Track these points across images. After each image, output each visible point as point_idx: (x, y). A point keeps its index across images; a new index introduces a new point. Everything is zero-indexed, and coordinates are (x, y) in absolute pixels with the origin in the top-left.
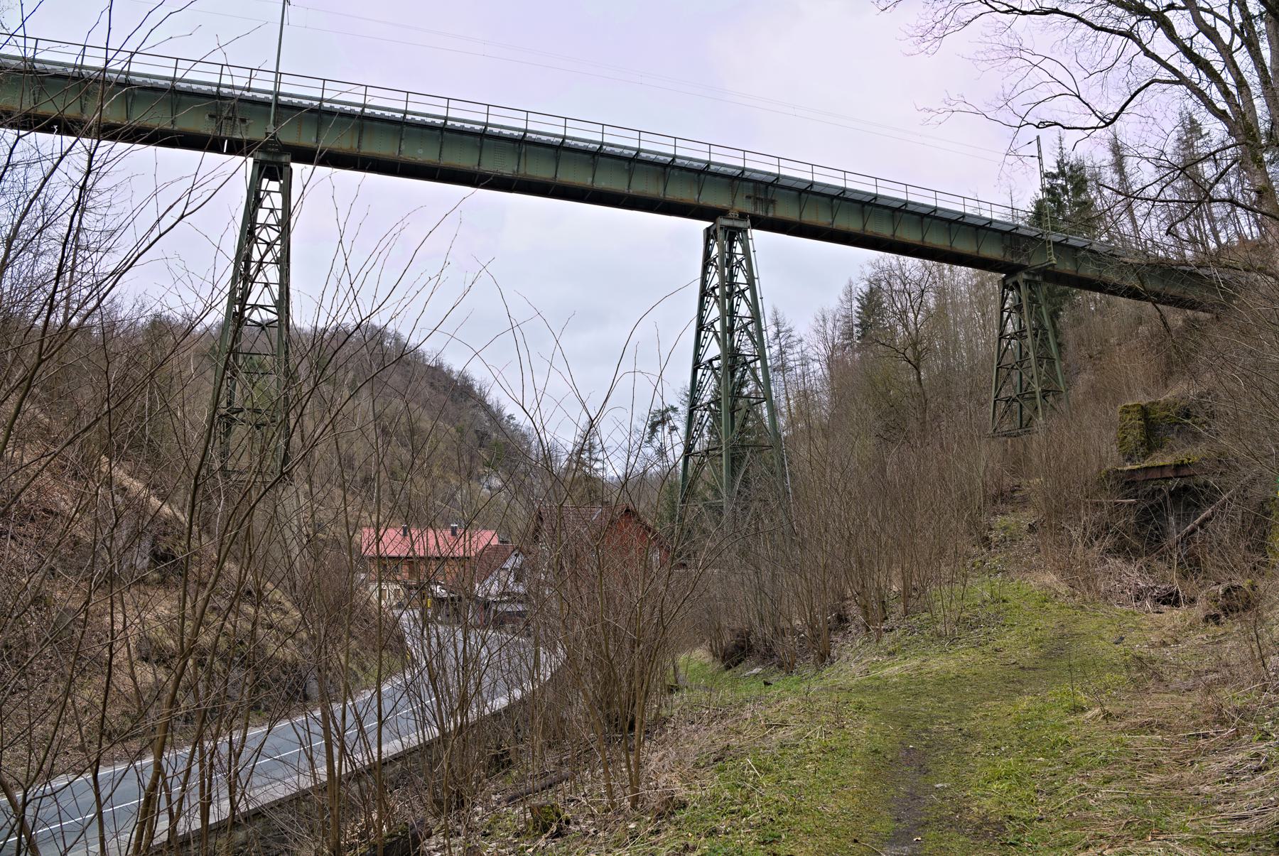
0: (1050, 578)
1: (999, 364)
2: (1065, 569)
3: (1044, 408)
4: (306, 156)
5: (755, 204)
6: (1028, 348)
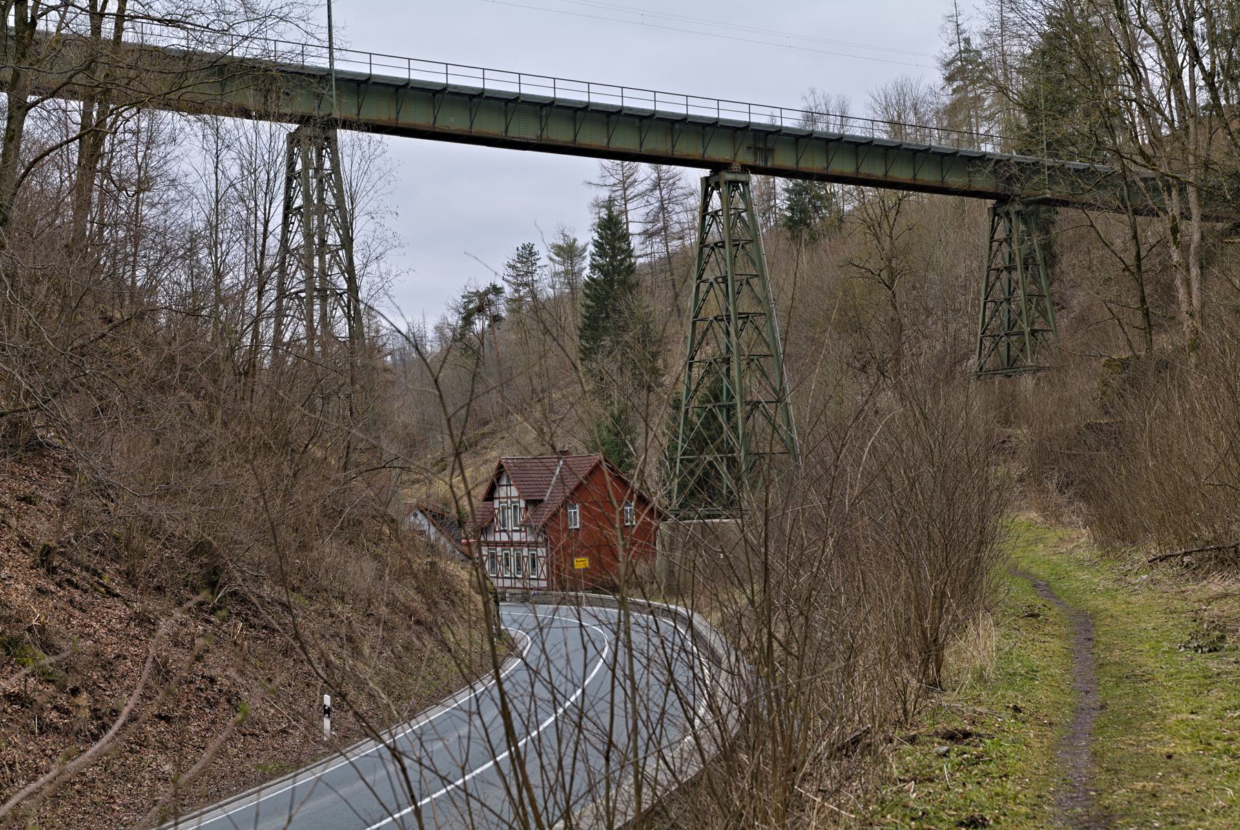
0: (1033, 515)
1: (986, 299)
2: (1043, 510)
3: (1033, 346)
4: (347, 125)
5: (755, 154)
6: (1017, 283)
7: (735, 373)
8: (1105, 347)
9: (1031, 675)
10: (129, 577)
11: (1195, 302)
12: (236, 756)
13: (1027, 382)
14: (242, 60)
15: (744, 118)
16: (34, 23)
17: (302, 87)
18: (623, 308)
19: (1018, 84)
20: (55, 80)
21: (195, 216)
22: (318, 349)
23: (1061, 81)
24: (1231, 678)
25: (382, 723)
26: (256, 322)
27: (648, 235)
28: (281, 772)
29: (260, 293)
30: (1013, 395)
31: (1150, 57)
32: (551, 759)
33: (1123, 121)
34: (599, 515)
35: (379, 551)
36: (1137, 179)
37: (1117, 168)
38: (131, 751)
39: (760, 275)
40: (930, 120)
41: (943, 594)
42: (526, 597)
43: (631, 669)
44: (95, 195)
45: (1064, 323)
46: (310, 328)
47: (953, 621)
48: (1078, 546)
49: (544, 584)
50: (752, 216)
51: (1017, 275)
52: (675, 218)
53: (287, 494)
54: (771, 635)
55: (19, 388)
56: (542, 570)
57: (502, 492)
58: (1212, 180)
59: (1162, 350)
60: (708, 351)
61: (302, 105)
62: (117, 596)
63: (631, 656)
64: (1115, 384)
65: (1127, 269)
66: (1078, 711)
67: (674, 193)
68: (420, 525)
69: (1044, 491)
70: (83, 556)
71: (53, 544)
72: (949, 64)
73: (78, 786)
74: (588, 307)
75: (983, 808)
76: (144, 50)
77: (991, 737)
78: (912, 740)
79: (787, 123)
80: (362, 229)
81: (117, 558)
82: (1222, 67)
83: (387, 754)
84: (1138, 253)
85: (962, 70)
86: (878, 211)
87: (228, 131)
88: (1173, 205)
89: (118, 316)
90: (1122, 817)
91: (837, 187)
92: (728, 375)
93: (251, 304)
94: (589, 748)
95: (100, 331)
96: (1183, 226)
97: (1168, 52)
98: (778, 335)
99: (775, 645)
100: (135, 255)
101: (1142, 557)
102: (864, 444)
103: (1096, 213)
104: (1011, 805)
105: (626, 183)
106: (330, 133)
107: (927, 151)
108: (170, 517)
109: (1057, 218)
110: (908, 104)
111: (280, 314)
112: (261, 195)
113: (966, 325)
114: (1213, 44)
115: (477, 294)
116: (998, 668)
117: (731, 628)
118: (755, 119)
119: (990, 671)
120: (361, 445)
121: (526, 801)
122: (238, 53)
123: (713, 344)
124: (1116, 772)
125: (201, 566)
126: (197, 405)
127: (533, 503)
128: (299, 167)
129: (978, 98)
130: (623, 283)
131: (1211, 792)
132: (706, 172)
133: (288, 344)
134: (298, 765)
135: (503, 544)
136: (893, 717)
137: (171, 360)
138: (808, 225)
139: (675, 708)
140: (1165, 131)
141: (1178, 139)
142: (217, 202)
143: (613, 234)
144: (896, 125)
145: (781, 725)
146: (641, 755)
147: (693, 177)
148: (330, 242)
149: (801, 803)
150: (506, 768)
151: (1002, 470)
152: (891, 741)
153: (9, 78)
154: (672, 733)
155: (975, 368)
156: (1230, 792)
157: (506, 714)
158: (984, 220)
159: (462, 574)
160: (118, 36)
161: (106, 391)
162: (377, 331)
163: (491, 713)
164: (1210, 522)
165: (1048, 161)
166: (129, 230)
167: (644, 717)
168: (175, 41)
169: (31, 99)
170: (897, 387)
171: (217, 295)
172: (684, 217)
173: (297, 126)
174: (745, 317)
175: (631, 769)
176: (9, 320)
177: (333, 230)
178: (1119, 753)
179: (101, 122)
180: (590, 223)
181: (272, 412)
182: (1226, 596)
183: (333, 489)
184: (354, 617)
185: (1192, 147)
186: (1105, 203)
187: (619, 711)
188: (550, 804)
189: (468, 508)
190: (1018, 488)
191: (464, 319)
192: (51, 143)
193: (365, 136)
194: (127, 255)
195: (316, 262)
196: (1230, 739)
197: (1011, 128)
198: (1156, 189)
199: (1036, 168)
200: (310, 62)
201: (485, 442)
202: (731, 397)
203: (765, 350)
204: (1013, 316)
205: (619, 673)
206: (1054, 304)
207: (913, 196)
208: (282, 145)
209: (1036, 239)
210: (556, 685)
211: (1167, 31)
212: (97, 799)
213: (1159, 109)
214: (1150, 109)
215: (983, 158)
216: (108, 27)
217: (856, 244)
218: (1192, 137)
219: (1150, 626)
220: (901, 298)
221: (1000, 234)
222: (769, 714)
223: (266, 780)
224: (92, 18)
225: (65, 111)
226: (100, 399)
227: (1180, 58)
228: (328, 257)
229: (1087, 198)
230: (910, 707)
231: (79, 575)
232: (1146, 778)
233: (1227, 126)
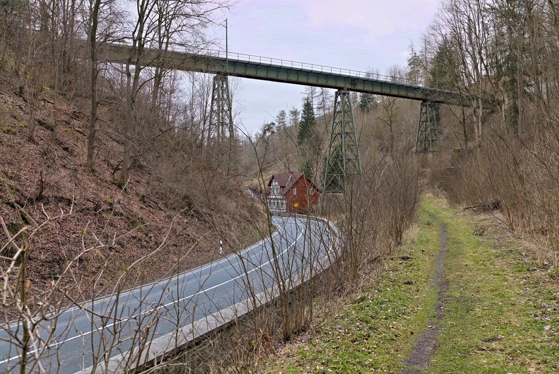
2: (433, 193)
3: (432, 145)
4: (231, 74)
7: (343, 150)
8: (453, 146)
9: (428, 241)
10: (166, 205)
11: (480, 133)
12: (195, 257)
13: (430, 155)
14: (201, 55)
15: (348, 74)
16: (143, 45)
17: (218, 63)
18: (311, 130)
19: (430, 67)
20: (149, 61)
21: (186, 100)
22: (220, 140)
23: (443, 66)
24: (485, 243)
25: (237, 249)
26: (203, 132)
27: (319, 108)
28: (207, 262)
29: (204, 123)
30: (426, 159)
31: (469, 60)
32: (286, 261)
33: (461, 78)
34: (302, 191)
35: (237, 200)
36: (464, 96)
37: (459, 92)
38: (166, 254)
39: (352, 121)
40: (404, 76)
41: (403, 217)
42: (279, 215)
43: (310, 236)
44: (159, 94)
45: (441, 138)
46: (219, 134)
47: (406, 225)
48: (443, 204)
49: (285, 211)
50: (350, 103)
51: (428, 123)
52: (327, 103)
53: (211, 182)
54: (352, 227)
55: (136, 150)
56: (285, 206)
57: (273, 184)
58: (486, 97)
59: (470, 147)
60: (336, 143)
61: (218, 69)
62: (162, 210)
63: (310, 232)
64: (456, 157)
65: (460, 122)
66: (441, 252)
67: (327, 96)
68: (249, 192)
69: (434, 188)
70: (153, 198)
71: (145, 195)
72: (409, 60)
73: (151, 263)
74: (300, 129)
75: (412, 279)
76: (173, 53)
77: (415, 259)
78: (392, 259)
79: (361, 76)
80: (234, 105)
81: (162, 199)
82: (490, 64)
83: (238, 258)
84: (464, 118)
85: (413, 62)
86: (388, 103)
87: (196, 76)
88: (474, 104)
89: (164, 129)
90: (452, 282)
91: (375, 96)
92: (341, 150)
93: (202, 127)
94: (297, 258)
95: (159, 134)
96: (477, 110)
97: (474, 59)
98: (357, 139)
99: (353, 230)
100: (169, 112)
101: (462, 208)
102: (381, 172)
103: (452, 106)
104: (420, 278)
105: (312, 93)
106: (226, 77)
107: (402, 85)
108: (177, 188)
109: (441, 107)
110: (397, 72)
111: (210, 129)
112: (205, 95)
113: (412, 138)
114: (487, 57)
115: (268, 125)
116: (418, 239)
117: (340, 226)
118: (352, 75)
119: (416, 240)
120: (232, 169)
121: (278, 272)
122: (200, 53)
123: (337, 141)
124: (451, 269)
125: (186, 202)
126: (185, 156)
127: (283, 187)
128: (216, 87)
129: (418, 70)
130: (311, 123)
131: (478, 276)
132: (337, 90)
133: (212, 138)
134: (212, 260)
135: (273, 199)
136: (387, 252)
137: (179, 142)
138: (367, 107)
139: (322, 248)
140: (473, 82)
141: (476, 84)
142: (193, 97)
143: (309, 108)
144: (393, 77)
145: (354, 253)
146: (312, 260)
147: (333, 91)
148: (225, 109)
149: (359, 276)
150: (273, 263)
151: (422, 181)
152: (386, 259)
153: (136, 61)
154: (322, 255)
155: (415, 151)
156: (483, 276)
157: (273, 247)
158: (419, 106)
159: (261, 207)
160: (166, 49)
161: (160, 151)
162: (238, 135)
163: (269, 247)
164: (482, 198)
165: (438, 90)
166: (167, 104)
167: (313, 250)
168: (182, 50)
169: (142, 67)
170: (392, 155)
171: (192, 124)
172: (329, 103)
173: (216, 75)
174: (347, 134)
175: (309, 265)
176: (134, 130)
177: (226, 105)
178: (452, 264)
179: (161, 73)
180: (302, 104)
181: (207, 158)
182: (485, 220)
183: (224, 181)
184: (229, 219)
185: (480, 87)
186: (454, 102)
187: (306, 248)
188: (285, 273)
189: (264, 188)
190: (426, 186)
191: (263, 132)
192: (147, 80)
193: (236, 78)
194: (167, 112)
195: (221, 115)
196: (484, 261)
197: (428, 79)
198: (470, 99)
199: (435, 92)
200: (220, 56)
201: (268, 169)
202: (342, 157)
203: (353, 144)
204: (427, 136)
205: (306, 237)
206: (439, 132)
207: (398, 99)
208: (212, 80)
209: (434, 113)
210: (288, 240)
211: (474, 52)
212: (157, 267)
213: (471, 75)
214: (468, 76)
215: (419, 88)
216: (164, 46)
217: (381, 113)
218: (480, 84)
219: (463, 228)
220: (394, 129)
221: (424, 111)
222: (350, 250)
223: (203, 264)
224: (159, 44)
225: (151, 70)
226: (159, 153)
227: (477, 61)
228: (224, 113)
229: (450, 101)
230: (392, 250)
231: (152, 204)
232: (459, 271)
233: (491, 81)
